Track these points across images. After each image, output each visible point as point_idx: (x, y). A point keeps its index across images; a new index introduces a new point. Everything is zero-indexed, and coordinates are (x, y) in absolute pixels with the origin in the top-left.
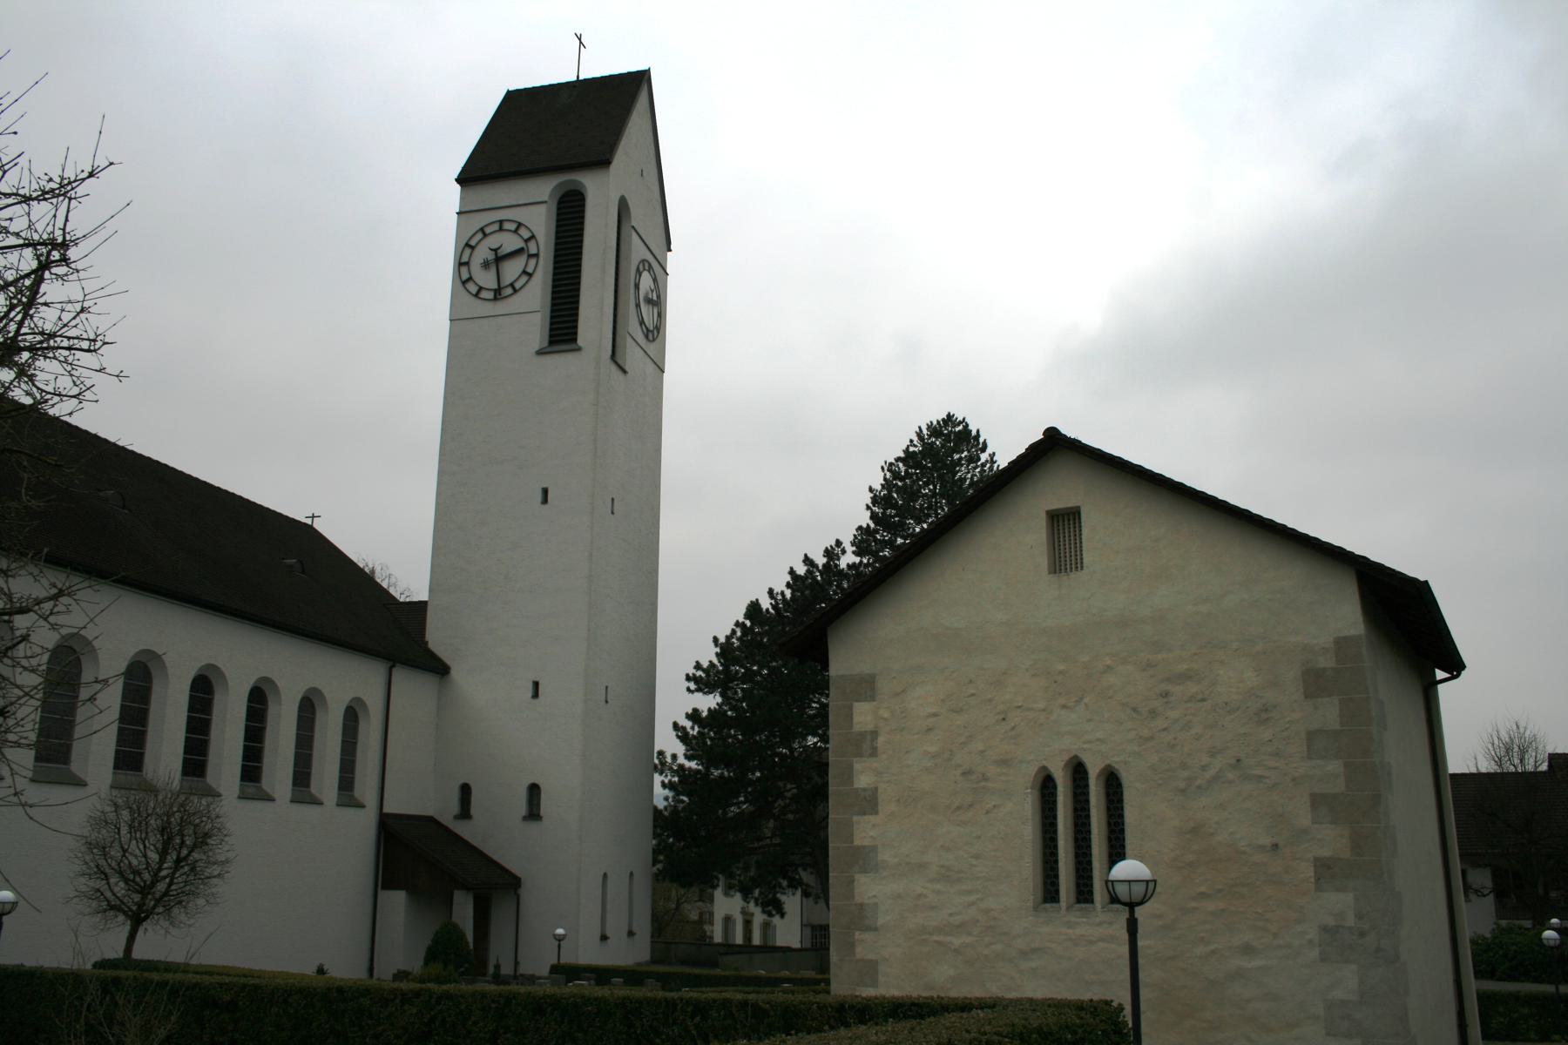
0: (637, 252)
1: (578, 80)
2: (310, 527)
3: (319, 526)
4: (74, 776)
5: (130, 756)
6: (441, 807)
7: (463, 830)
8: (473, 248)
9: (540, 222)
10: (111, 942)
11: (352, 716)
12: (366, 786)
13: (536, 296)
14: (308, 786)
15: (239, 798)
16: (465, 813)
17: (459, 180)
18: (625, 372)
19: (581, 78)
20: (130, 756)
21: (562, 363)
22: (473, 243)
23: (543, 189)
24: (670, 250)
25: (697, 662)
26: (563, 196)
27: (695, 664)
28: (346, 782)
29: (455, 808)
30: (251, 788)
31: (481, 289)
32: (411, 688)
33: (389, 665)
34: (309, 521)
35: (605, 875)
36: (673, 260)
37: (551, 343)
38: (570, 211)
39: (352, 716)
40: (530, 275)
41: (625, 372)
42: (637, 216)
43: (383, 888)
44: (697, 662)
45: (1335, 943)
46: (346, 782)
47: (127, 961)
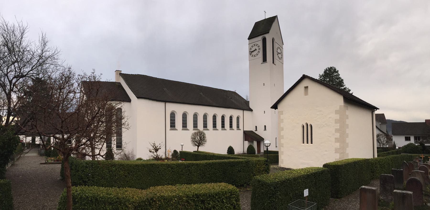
0: (276, 46)
1: (265, 19)
2: (235, 92)
3: (237, 92)
4: (217, 129)
5: (195, 125)
6: (253, 129)
7: (256, 132)
8: (251, 49)
9: (260, 44)
10: (195, 149)
11: (238, 118)
12: (241, 127)
13: (261, 55)
14: (232, 128)
15: (222, 130)
16: (256, 130)
17: (248, 39)
18: (275, 65)
19: (266, 18)
20: (195, 125)
21: (265, 64)
22: (251, 48)
23: (260, 38)
24: (283, 45)
25: (272, 108)
26: (263, 39)
27: (251, 106)
28: (238, 127)
29: (255, 129)
30: (223, 128)
31: (255, 55)
32: (246, 113)
33: (372, 111)
34: (235, 91)
35: (276, 138)
36: (284, 46)
37: (263, 62)
38: (264, 40)
39: (238, 118)
40: (259, 52)
41: (275, 65)
42: (276, 40)
43: (245, 141)
44: (272, 108)
45: (337, 140)
46: (238, 127)
47: (197, 151)
